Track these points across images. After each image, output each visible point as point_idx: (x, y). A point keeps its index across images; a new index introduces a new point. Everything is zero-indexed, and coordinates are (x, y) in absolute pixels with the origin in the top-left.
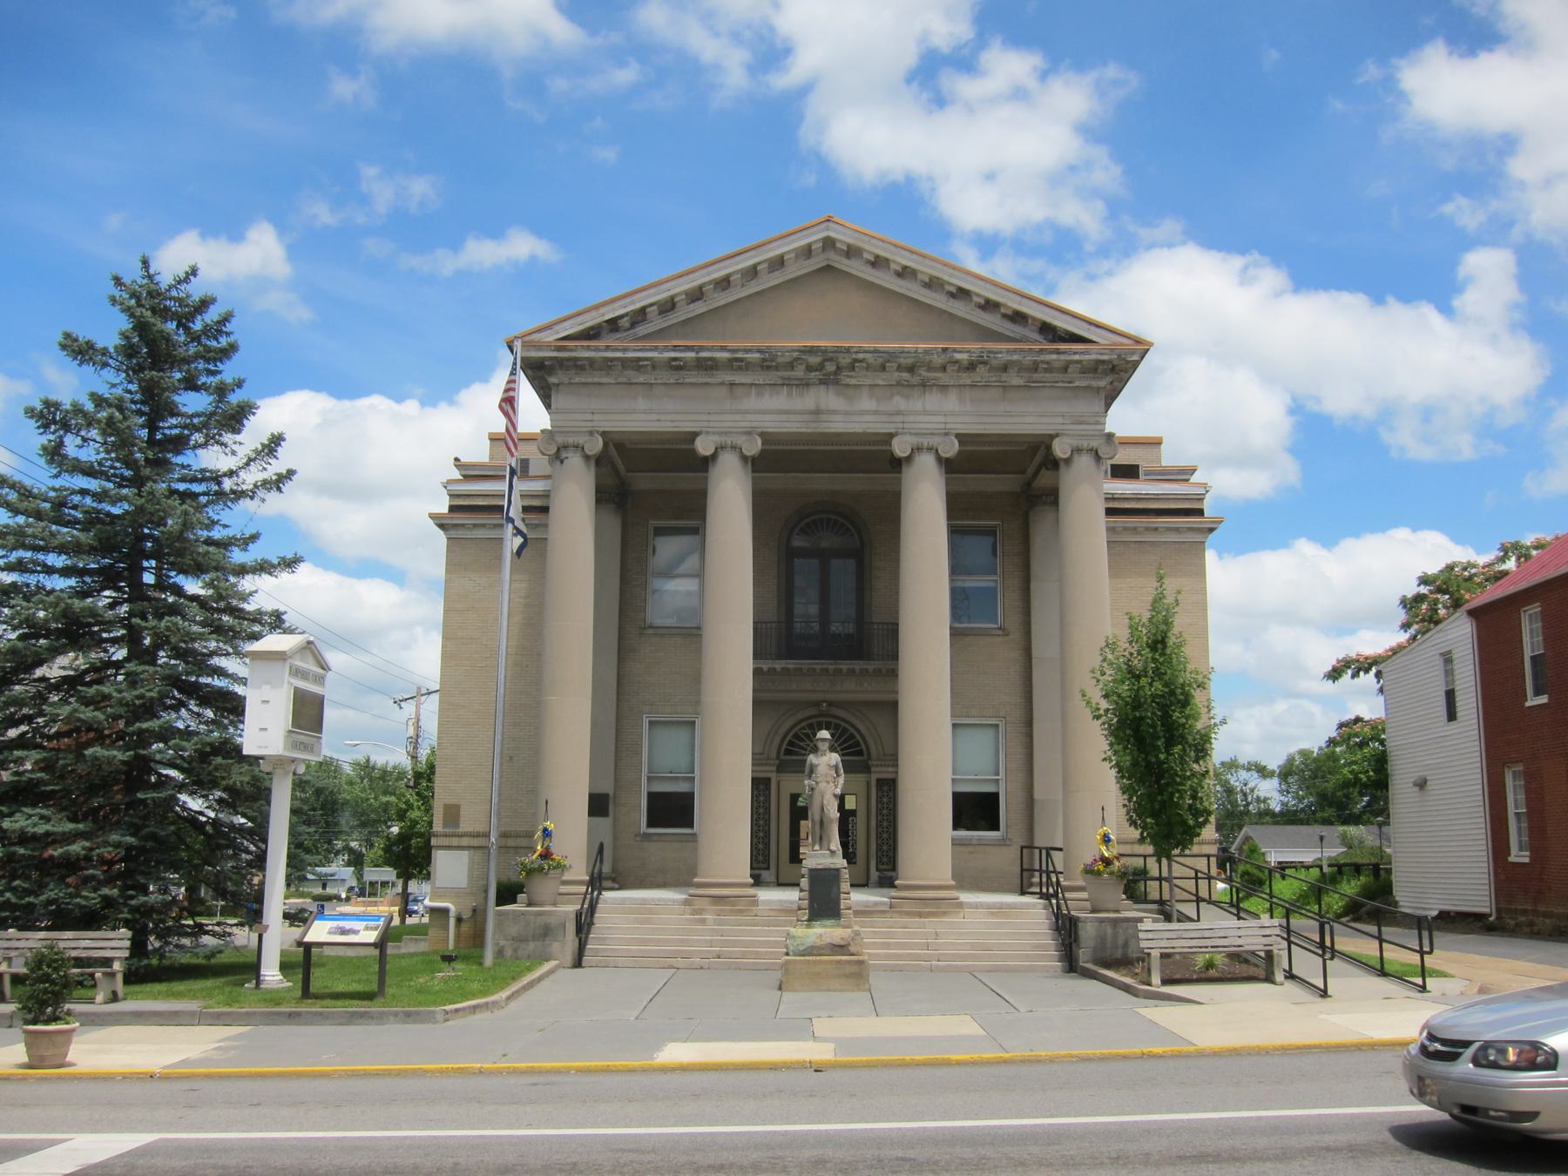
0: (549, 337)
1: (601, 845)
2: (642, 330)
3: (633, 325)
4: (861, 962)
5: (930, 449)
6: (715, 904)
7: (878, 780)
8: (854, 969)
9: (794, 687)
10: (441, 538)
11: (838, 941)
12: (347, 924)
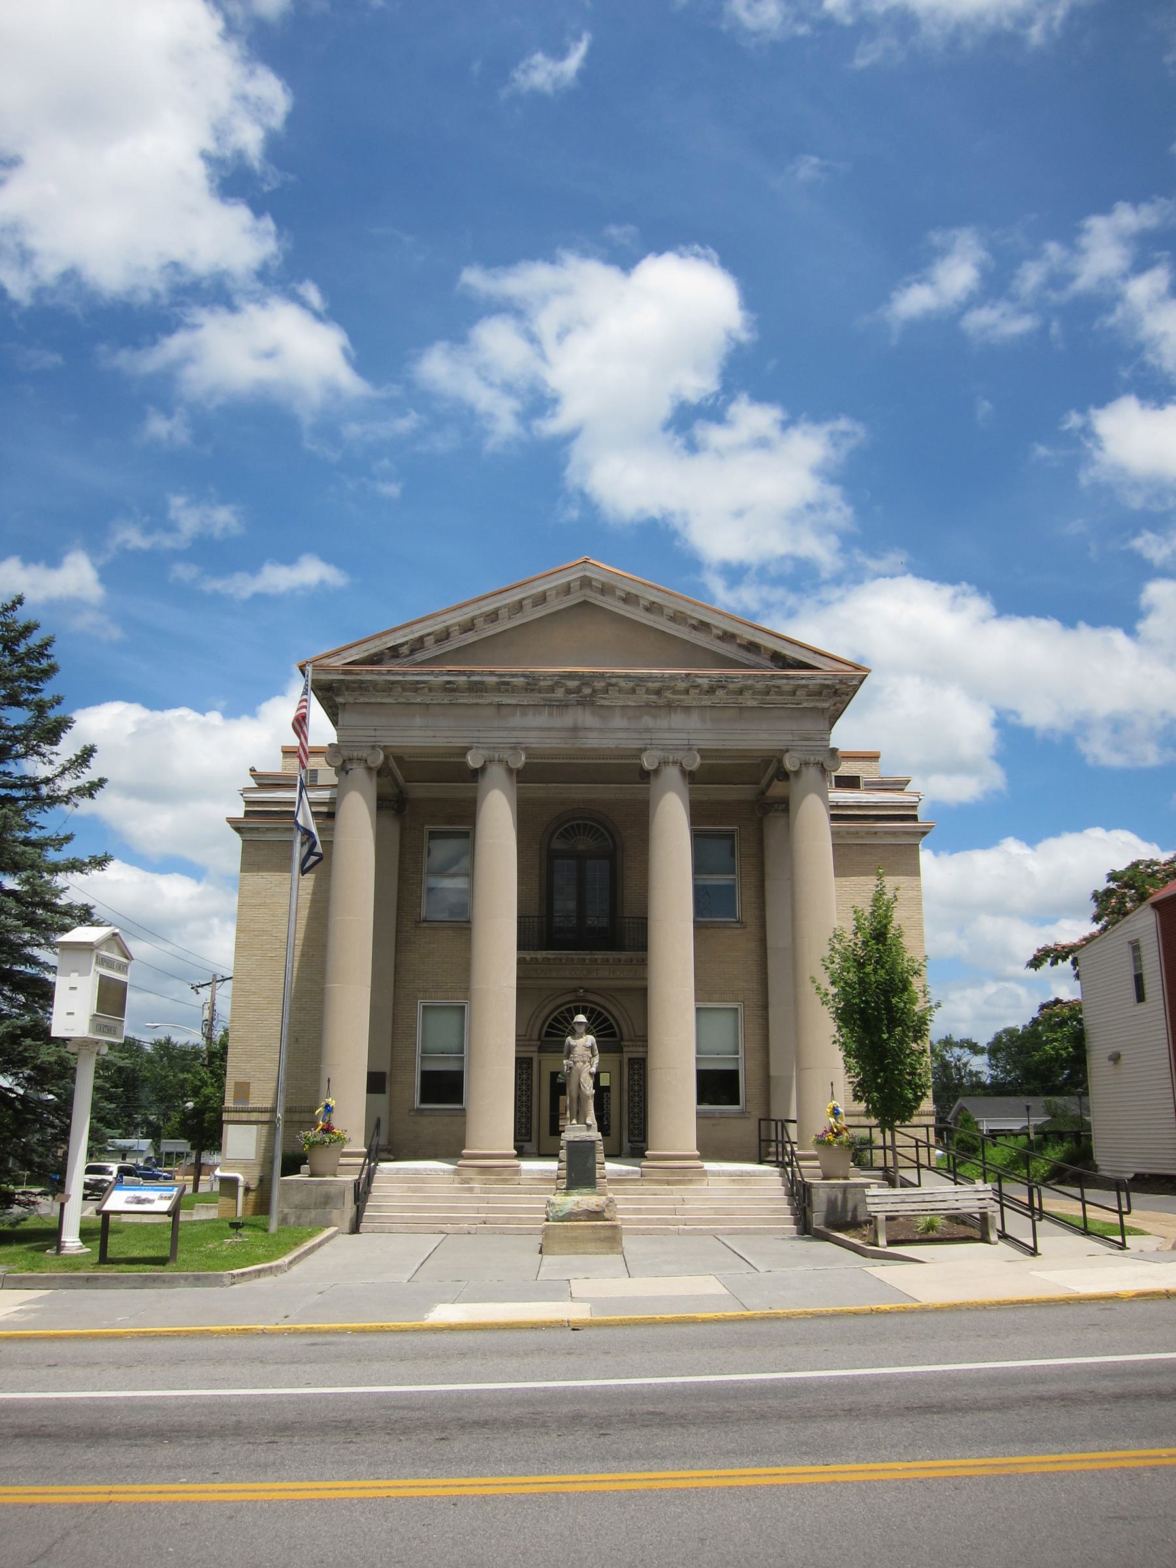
0: (337, 662)
1: (379, 1120)
2: (420, 656)
3: (412, 651)
4: (616, 1227)
5: (675, 763)
7: (630, 1059)
8: (608, 1233)
10: (237, 840)
11: (593, 1207)
12: (143, 1194)
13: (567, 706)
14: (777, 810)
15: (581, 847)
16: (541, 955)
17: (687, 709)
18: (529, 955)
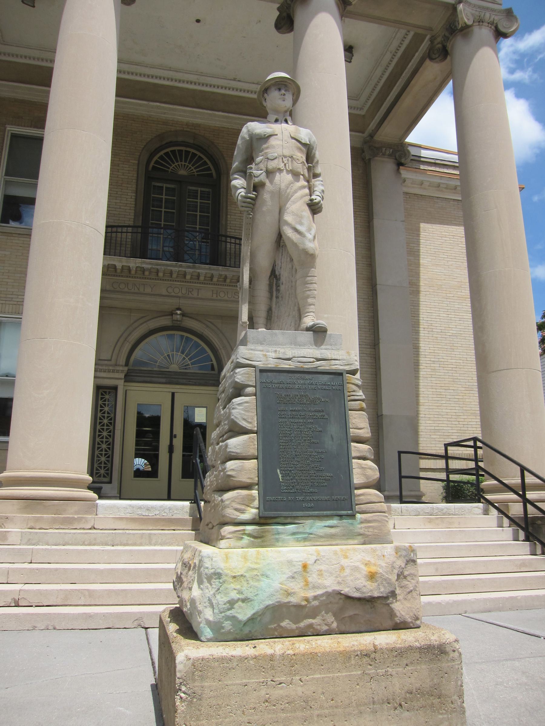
4: (438, 652)
6: (25, 510)
8: (419, 675)
9: (148, 290)
11: (357, 584)
14: (384, 154)
15: (182, 172)
16: (134, 263)
18: (119, 262)
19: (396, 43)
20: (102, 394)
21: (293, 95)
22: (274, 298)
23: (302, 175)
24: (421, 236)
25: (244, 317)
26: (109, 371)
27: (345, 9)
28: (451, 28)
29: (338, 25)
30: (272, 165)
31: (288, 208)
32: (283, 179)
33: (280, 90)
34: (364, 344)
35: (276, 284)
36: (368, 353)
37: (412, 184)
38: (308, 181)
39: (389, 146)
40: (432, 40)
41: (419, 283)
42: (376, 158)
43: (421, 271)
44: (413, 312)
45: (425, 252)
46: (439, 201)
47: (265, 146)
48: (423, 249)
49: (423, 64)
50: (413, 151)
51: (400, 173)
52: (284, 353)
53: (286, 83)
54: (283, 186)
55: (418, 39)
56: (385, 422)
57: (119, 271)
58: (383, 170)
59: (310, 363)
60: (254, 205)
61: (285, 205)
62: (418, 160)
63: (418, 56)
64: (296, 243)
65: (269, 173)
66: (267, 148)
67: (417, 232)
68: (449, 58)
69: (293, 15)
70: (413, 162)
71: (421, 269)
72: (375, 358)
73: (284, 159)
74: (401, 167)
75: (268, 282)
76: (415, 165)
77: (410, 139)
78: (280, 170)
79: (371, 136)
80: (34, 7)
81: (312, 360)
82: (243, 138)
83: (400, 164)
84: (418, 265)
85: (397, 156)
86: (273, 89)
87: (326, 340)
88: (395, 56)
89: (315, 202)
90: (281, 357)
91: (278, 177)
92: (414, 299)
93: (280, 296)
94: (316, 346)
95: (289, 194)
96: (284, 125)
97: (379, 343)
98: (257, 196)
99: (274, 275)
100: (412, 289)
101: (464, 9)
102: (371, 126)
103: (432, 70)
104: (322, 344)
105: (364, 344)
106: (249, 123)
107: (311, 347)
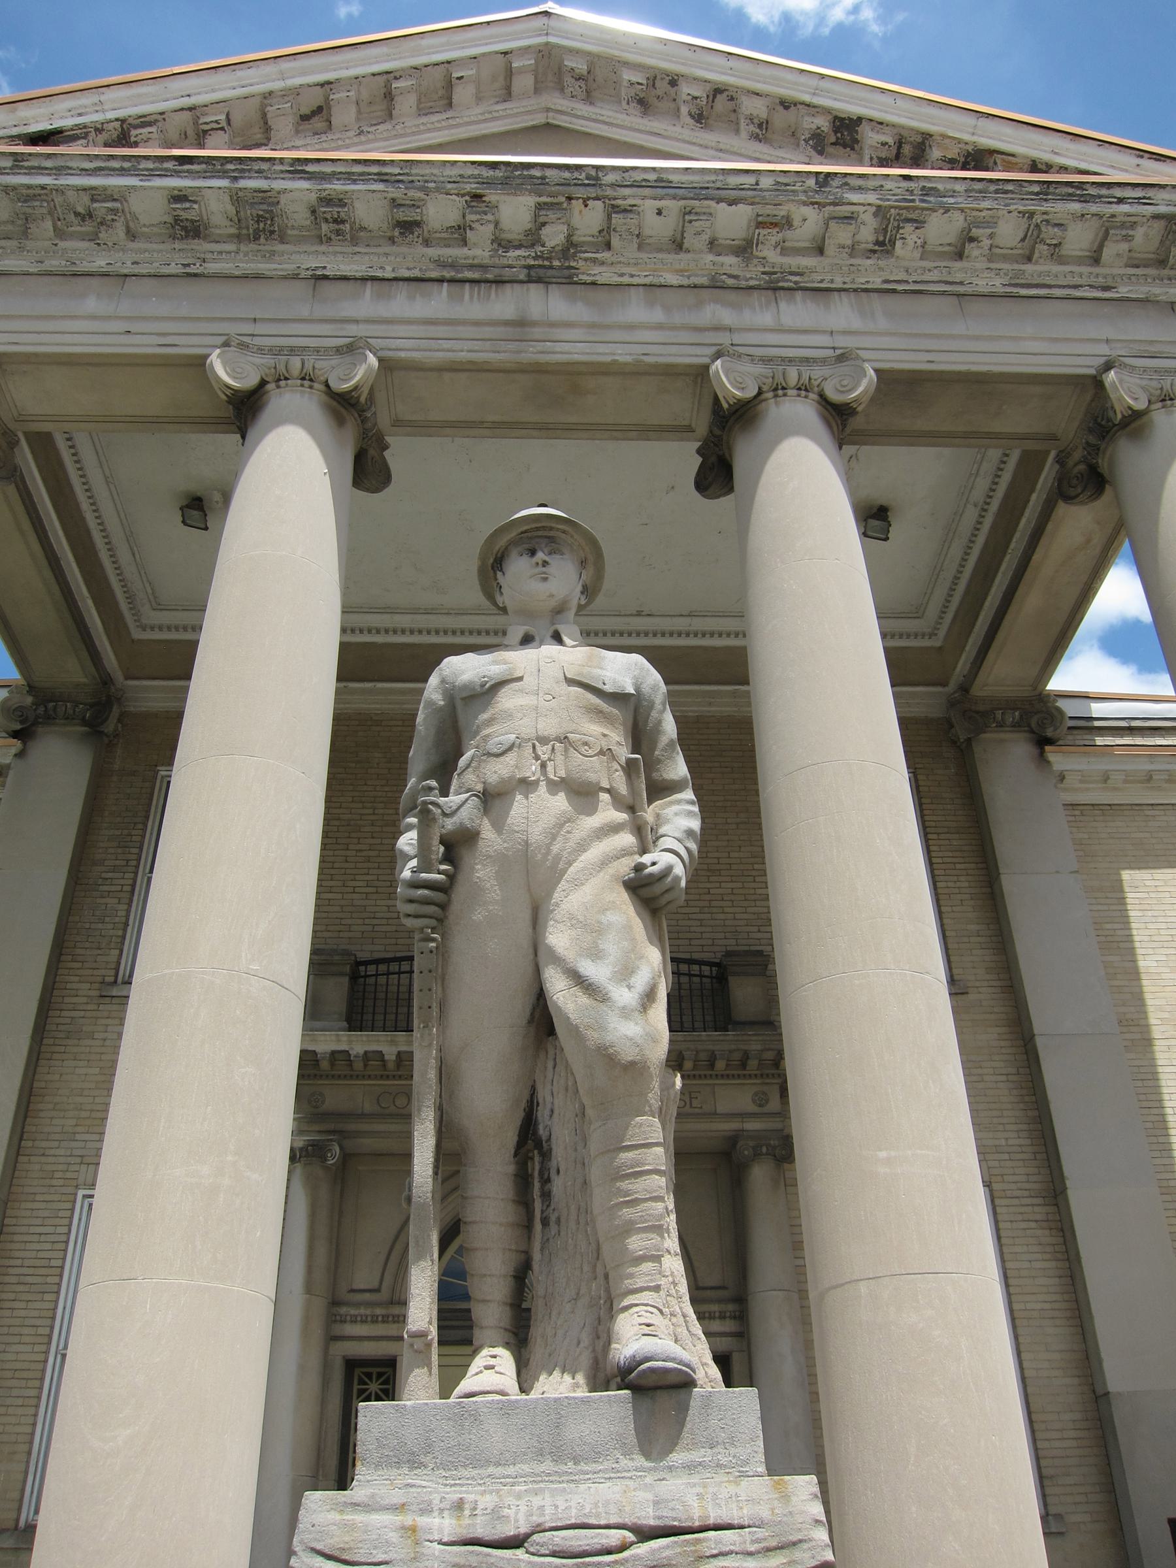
5: (803, 388)
13: (499, 282)
14: (1001, 725)
17: (822, 292)
19: (982, 484)
20: (361, 1382)
21: (583, 563)
22: (538, 1226)
23: (608, 791)
24: (1128, 901)
25: (422, 1312)
26: (375, 1320)
27: (844, 426)
28: (1100, 425)
29: (832, 461)
30: (497, 771)
31: (557, 905)
32: (538, 812)
33: (533, 553)
34: (1026, 1193)
35: (541, 1173)
36: (1038, 1217)
37: (1081, 782)
38: (632, 809)
39: (1010, 705)
40: (1060, 460)
41: (1146, 1018)
42: (983, 736)
43: (1145, 989)
44: (1142, 1097)
45: (1146, 938)
46: (1157, 813)
47: (484, 716)
48: (1140, 934)
49: (1050, 516)
50: (1070, 709)
51: (1048, 762)
52: (496, 1514)
53: (552, 533)
54: (536, 834)
55: (1030, 465)
56: (1120, 1414)
57: (391, 1066)
58: (1006, 764)
59: (609, 1552)
60: (443, 907)
61: (549, 895)
62: (1087, 727)
63: (1036, 500)
64: (577, 1027)
65: (492, 799)
66: (490, 722)
67: (1117, 894)
68: (1108, 489)
69: (731, 456)
70: (1075, 732)
71: (1144, 983)
72: (1062, 1230)
73: (540, 750)
74: (1047, 748)
75: (511, 1169)
76: (1081, 738)
77: (1058, 682)
78: (527, 786)
79: (964, 689)
80: (206, 529)
81: (614, 1537)
82: (431, 703)
83: (1043, 742)
84: (1134, 974)
85: (1033, 725)
86: (514, 554)
87: (688, 1426)
88: (986, 510)
89: (651, 875)
90: (480, 1532)
91: (518, 807)
92: (1137, 1063)
93: (553, 1218)
94: (647, 1455)
95: (558, 858)
96: (550, 650)
97: (1064, 1190)
98: (452, 877)
99: (530, 1140)
100: (1128, 1036)
101: (1121, 381)
102: (958, 669)
103: (1076, 523)
104: (672, 1445)
105: (1026, 1193)
106: (446, 660)
107: (625, 1462)
